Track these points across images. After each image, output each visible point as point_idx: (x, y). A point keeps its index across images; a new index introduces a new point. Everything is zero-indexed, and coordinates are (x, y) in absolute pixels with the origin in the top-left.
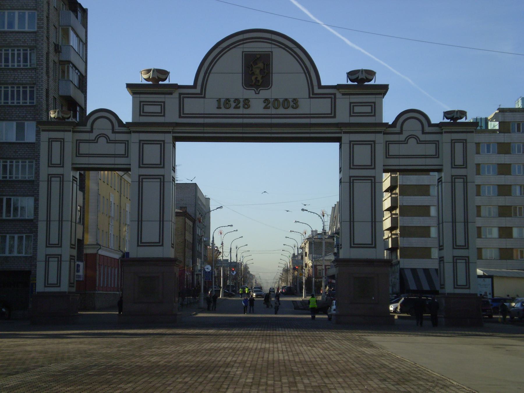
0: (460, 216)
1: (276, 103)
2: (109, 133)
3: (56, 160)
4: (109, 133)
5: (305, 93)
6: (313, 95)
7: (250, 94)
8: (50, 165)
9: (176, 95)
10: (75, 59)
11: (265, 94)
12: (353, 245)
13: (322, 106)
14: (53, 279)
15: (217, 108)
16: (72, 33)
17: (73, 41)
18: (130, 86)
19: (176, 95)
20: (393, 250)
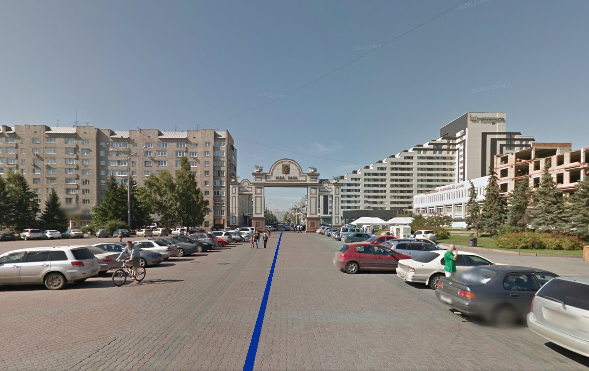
0: (337, 209)
1: (291, 178)
2: (247, 185)
3: (234, 192)
4: (247, 185)
5: (299, 175)
6: (301, 176)
7: (284, 175)
8: (233, 194)
9: (265, 176)
10: (234, 163)
11: (288, 175)
12: (311, 214)
13: (303, 179)
14: (234, 222)
15: (342, 270)
16: (233, 157)
17: (233, 158)
18: (252, 173)
19: (265, 176)
20: (545, 204)
